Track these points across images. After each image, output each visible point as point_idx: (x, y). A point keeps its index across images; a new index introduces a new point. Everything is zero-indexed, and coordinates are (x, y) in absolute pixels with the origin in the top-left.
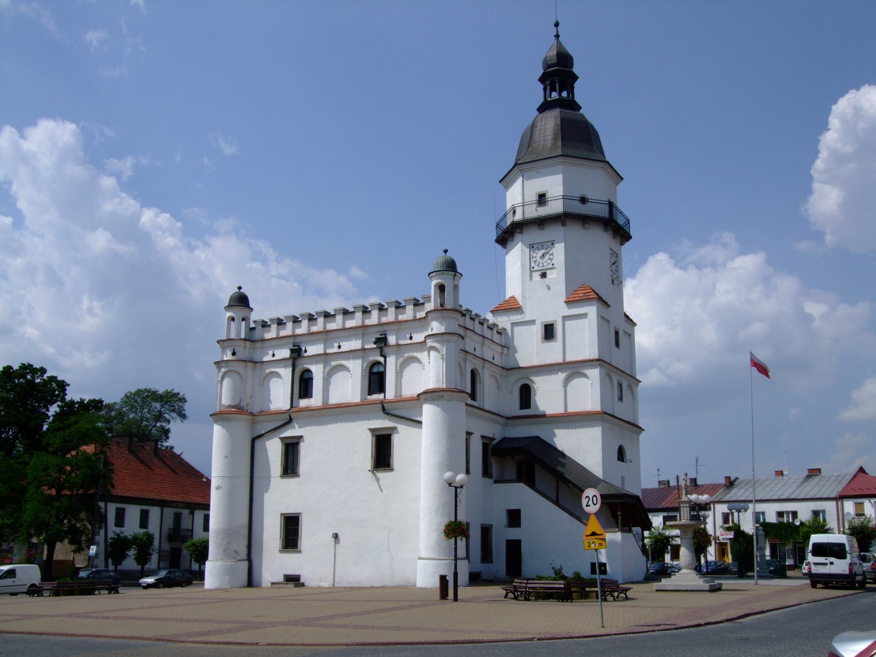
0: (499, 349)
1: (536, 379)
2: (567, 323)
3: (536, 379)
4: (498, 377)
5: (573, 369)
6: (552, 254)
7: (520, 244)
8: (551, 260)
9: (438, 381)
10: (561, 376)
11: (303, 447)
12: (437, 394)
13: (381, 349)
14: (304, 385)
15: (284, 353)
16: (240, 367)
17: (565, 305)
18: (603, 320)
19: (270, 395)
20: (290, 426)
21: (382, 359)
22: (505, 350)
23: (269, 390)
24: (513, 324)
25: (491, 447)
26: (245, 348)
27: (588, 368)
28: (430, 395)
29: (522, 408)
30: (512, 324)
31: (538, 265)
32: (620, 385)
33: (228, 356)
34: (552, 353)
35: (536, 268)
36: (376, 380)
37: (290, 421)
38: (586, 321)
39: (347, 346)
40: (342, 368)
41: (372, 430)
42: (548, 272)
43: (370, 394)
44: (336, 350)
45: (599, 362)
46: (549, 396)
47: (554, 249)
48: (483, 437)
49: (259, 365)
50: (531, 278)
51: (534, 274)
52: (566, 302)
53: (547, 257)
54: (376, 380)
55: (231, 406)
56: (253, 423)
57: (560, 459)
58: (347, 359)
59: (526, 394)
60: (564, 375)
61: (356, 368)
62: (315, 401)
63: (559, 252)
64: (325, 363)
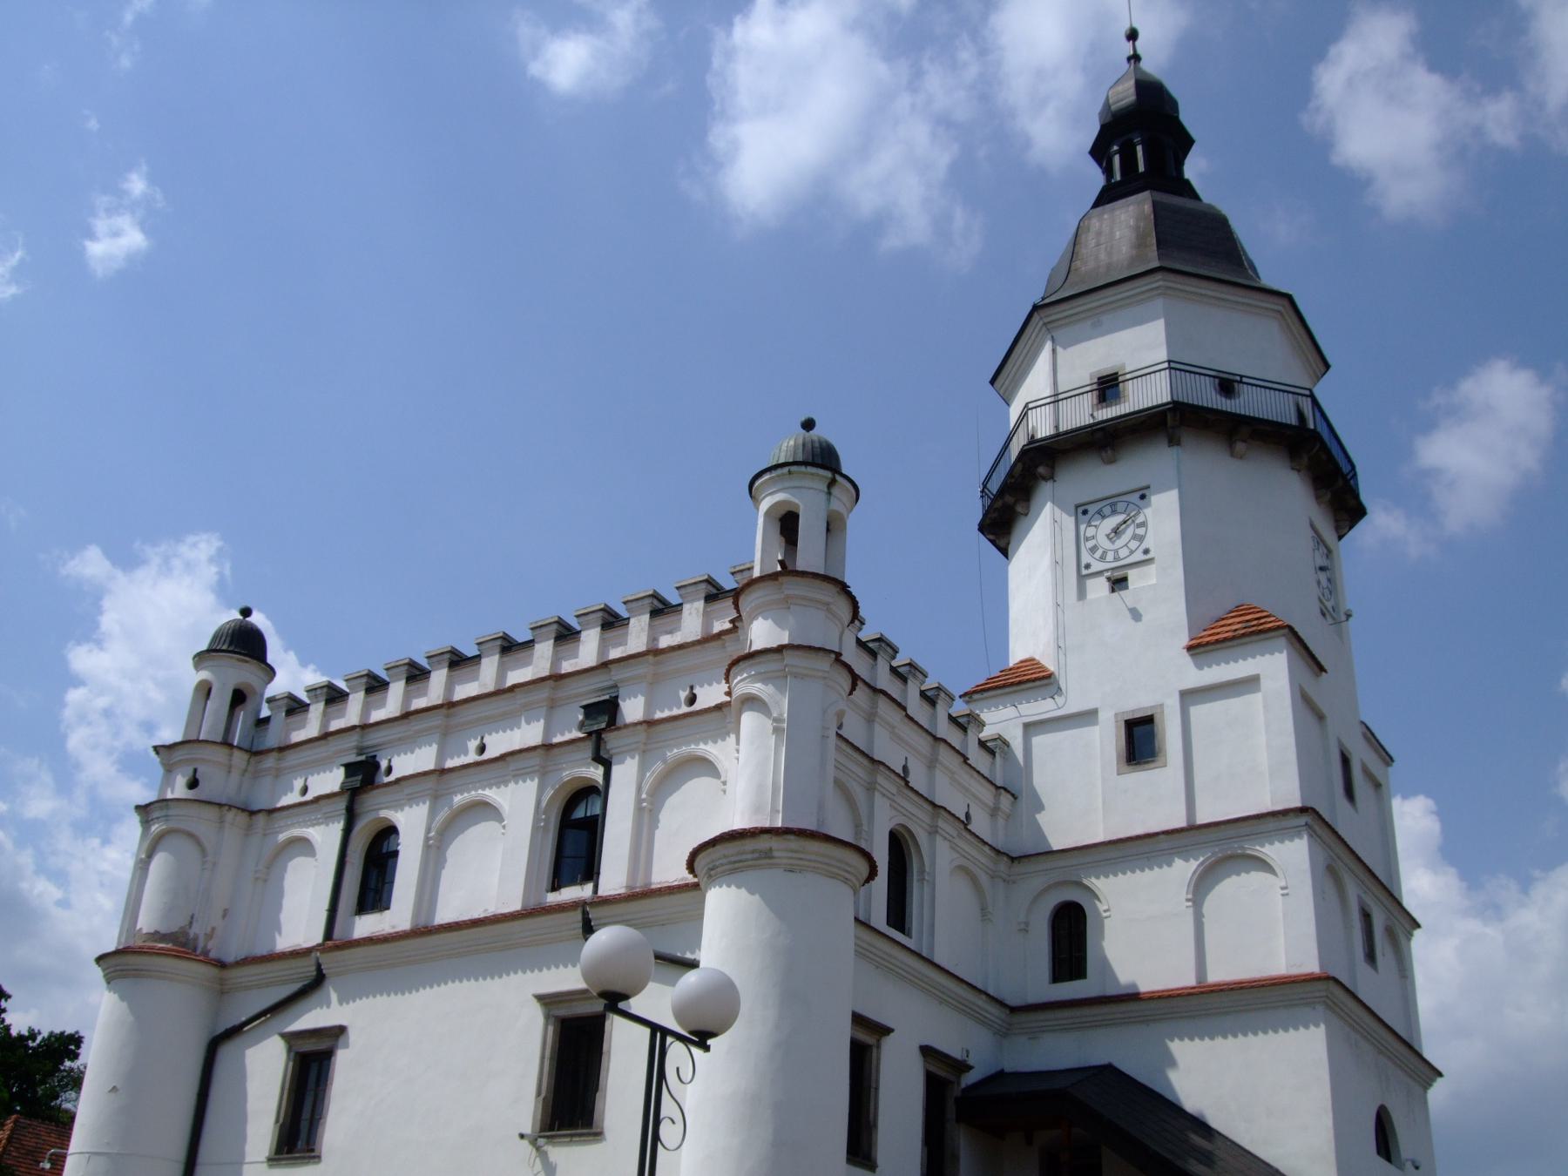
0: (986, 794)
1: (1100, 884)
2: (1197, 712)
3: (1100, 884)
4: (984, 879)
5: (1222, 846)
6: (1143, 524)
7: (1049, 505)
8: (1141, 539)
9: (757, 809)
10: (1183, 869)
11: (343, 1061)
12: (749, 845)
13: (596, 738)
14: (371, 871)
15: (330, 780)
16: (202, 823)
17: (1186, 658)
18: (1309, 708)
19: (279, 908)
20: (315, 997)
21: (596, 773)
22: (1005, 800)
23: (280, 894)
24: (1030, 728)
25: (957, 1092)
26: (229, 769)
27: (1269, 837)
28: (723, 854)
29: (1057, 977)
30: (1027, 726)
31: (1103, 558)
32: (1366, 917)
33: (179, 789)
34: (1153, 800)
35: (1097, 566)
36: (574, 839)
37: (317, 981)
38: (1254, 700)
39: (500, 743)
40: (485, 810)
41: (546, 1000)
42: (1132, 574)
43: (555, 887)
44: (472, 757)
45: (1307, 818)
46: (1145, 935)
47: (1148, 511)
48: (927, 1051)
49: (261, 820)
50: (1082, 593)
51: (1090, 583)
52: (1190, 648)
53: (1129, 532)
54: (574, 839)
55: (157, 936)
56: (222, 991)
57: (1197, 1140)
58: (501, 781)
59: (1071, 933)
60: (1193, 865)
61: (520, 804)
62: (398, 916)
63: (1163, 517)
64: (436, 798)
